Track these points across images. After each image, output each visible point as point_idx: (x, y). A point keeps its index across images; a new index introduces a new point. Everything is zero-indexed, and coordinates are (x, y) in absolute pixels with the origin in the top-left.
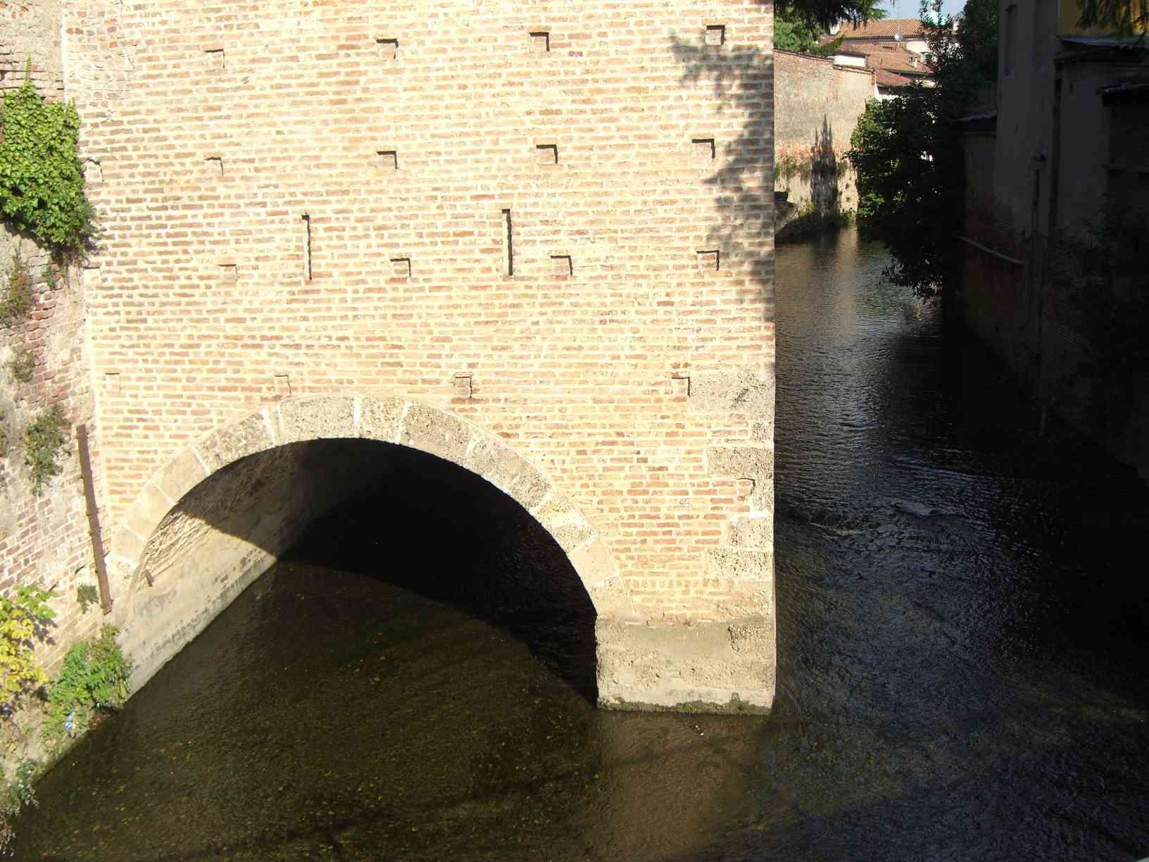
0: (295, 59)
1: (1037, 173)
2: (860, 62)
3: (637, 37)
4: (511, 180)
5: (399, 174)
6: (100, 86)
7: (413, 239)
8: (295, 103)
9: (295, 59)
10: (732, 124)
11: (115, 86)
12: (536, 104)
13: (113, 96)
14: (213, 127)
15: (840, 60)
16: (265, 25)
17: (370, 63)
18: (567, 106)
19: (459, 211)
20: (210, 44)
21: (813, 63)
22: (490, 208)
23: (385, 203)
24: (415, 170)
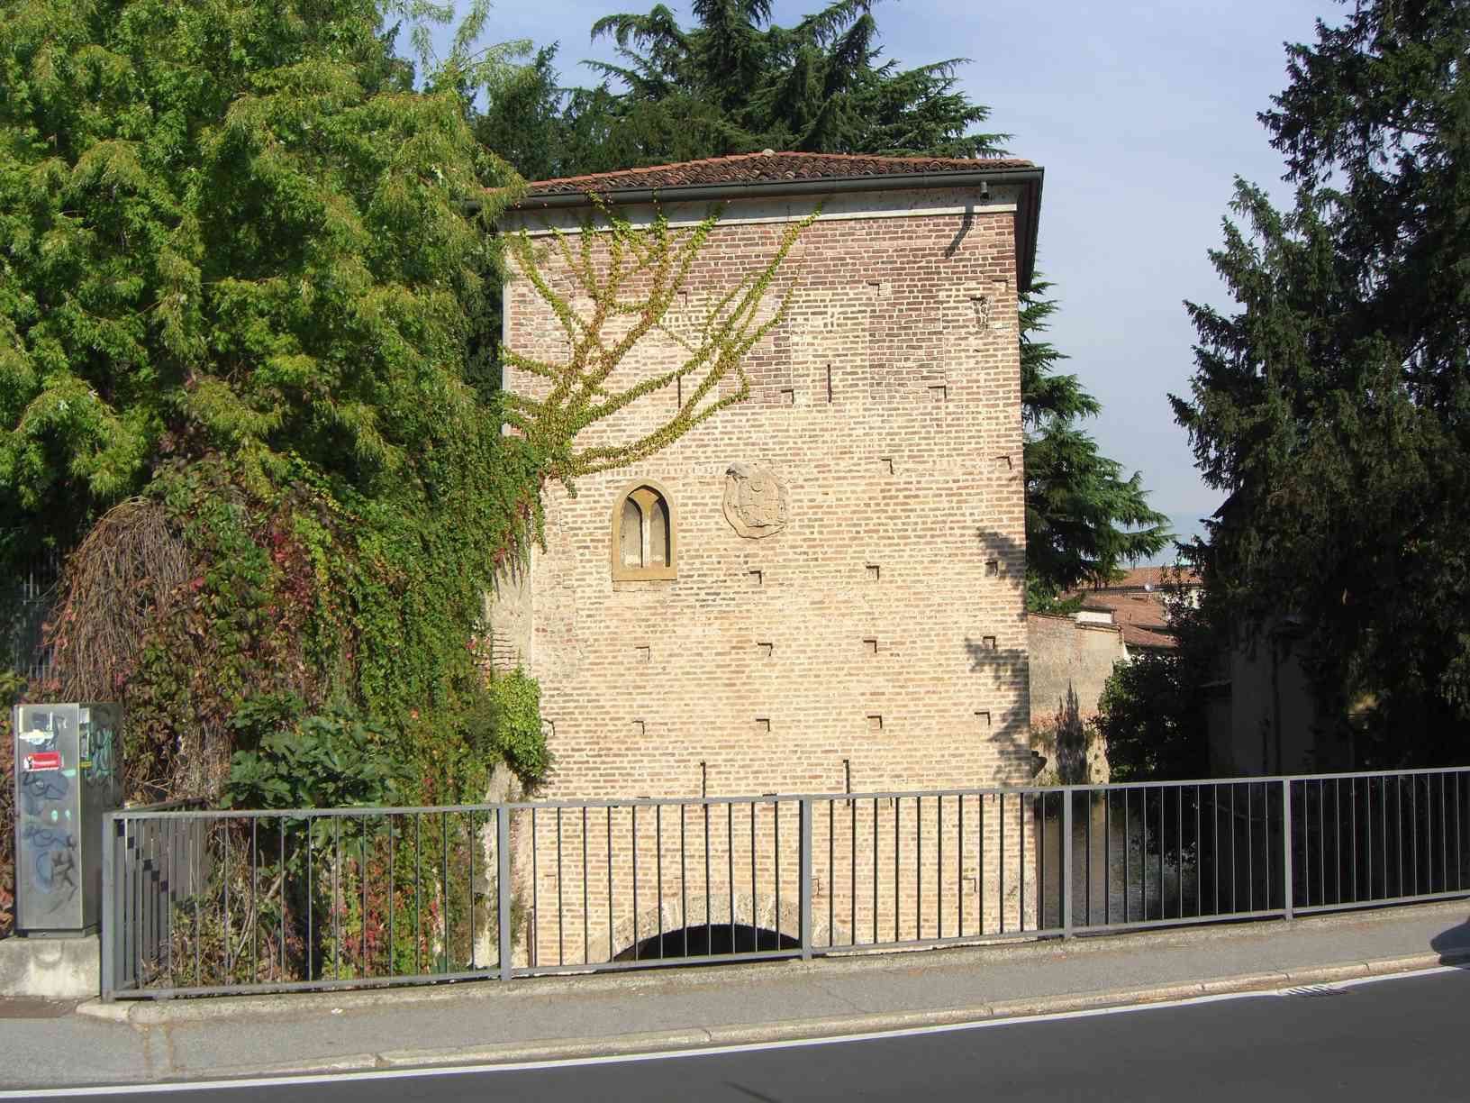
0: (700, 654)
1: (1265, 735)
2: (1105, 618)
3: (936, 644)
4: (850, 740)
5: (771, 735)
6: (557, 669)
7: (780, 780)
8: (699, 685)
9: (700, 654)
10: (1005, 700)
11: (569, 669)
12: (868, 689)
13: (567, 676)
14: (639, 700)
15: (1083, 616)
16: (680, 631)
17: (753, 661)
18: (889, 689)
19: (813, 761)
20: (640, 643)
21: (1053, 623)
22: (835, 759)
23: (761, 755)
24: (783, 732)
